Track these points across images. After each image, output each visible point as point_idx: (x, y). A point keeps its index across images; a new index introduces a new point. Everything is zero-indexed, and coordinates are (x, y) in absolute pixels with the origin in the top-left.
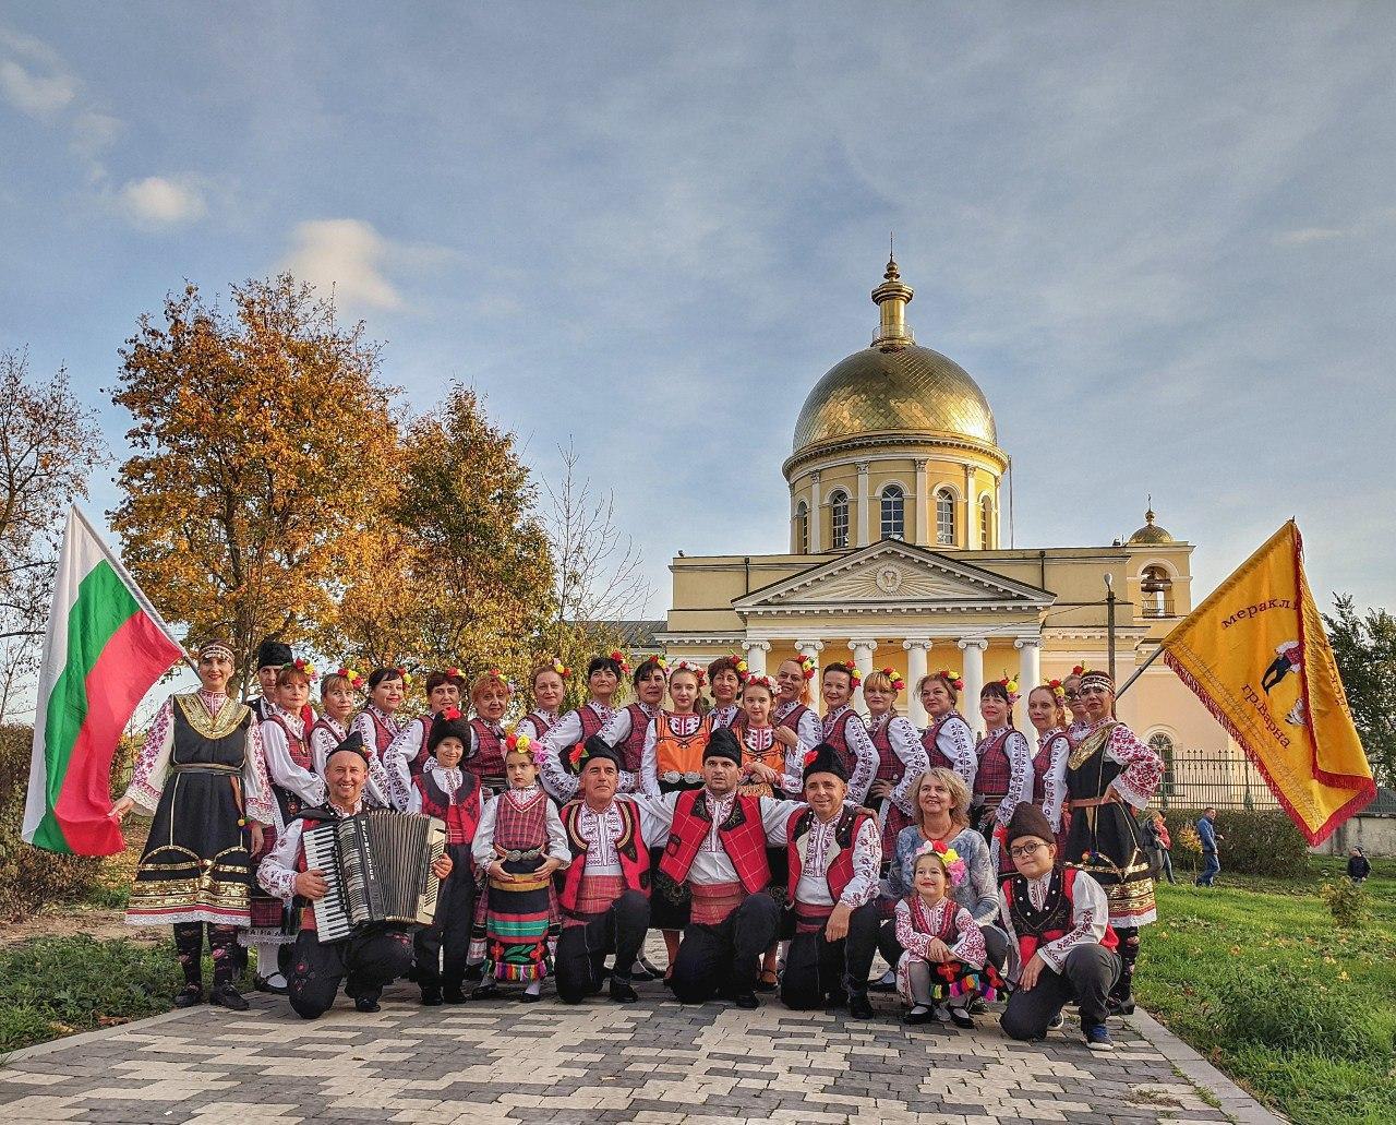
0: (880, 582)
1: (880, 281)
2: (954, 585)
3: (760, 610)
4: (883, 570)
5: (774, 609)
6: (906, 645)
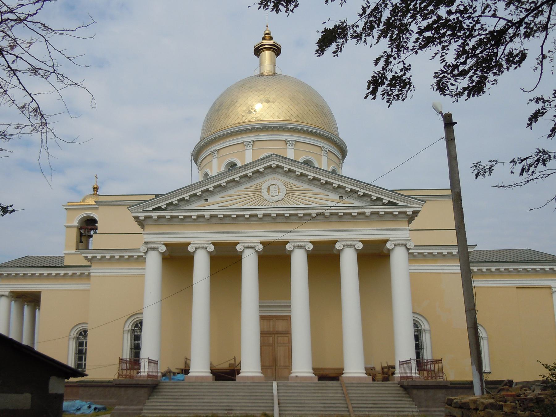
3: (155, 215)
5: (168, 214)
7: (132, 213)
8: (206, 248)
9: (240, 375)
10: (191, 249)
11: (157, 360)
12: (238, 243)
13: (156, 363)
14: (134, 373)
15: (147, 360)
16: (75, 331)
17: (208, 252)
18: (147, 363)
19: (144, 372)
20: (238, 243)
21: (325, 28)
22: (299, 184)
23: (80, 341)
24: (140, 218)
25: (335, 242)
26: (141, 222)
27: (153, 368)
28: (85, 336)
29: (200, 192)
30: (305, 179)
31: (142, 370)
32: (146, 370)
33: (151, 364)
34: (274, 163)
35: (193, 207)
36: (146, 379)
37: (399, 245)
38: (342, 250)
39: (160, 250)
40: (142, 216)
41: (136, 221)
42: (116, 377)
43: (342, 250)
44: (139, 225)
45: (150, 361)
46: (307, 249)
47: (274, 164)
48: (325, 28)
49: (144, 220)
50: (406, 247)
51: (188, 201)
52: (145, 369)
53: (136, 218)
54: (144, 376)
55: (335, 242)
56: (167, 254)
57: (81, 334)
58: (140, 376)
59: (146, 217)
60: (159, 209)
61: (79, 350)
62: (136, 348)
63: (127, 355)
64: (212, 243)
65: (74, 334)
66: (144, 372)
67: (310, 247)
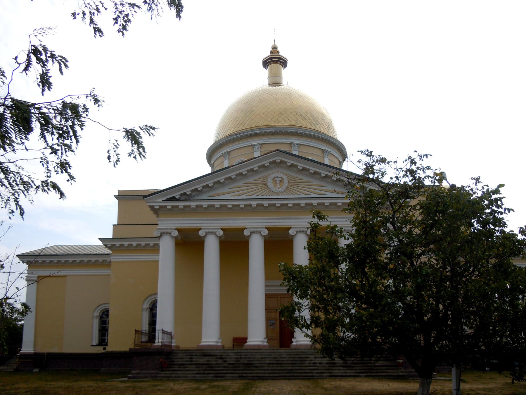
0: (270, 184)
1: (267, 54)
2: (330, 187)
3: (169, 204)
4: (273, 176)
5: (181, 204)
6: (291, 232)
7: (147, 203)
8: (171, 233)
9: (246, 344)
10: (246, 233)
11: (171, 332)
12: (245, 228)
13: (170, 334)
14: (149, 344)
15: (161, 331)
16: (99, 310)
17: (172, 237)
18: (160, 334)
19: (158, 342)
20: (245, 228)
21: (116, 196)
22: (300, 177)
23: (103, 319)
24: (155, 207)
25: (290, 228)
26: (156, 211)
27: (166, 341)
28: (107, 316)
29: (268, 163)
30: (307, 173)
31: (156, 341)
32: (160, 341)
33: (165, 335)
34: (278, 159)
35: (205, 197)
36: (160, 347)
37: (300, 232)
38: (295, 235)
39: (172, 234)
40: (157, 205)
41: (152, 210)
42: (133, 347)
43: (295, 235)
44: (154, 213)
45: (164, 332)
46: (263, 234)
47: (278, 159)
48: (116, 196)
49: (158, 209)
50: (171, 235)
51: (200, 192)
52: (159, 341)
53: (152, 208)
54: (158, 346)
55: (290, 228)
56: (179, 238)
57: (103, 313)
58: (155, 346)
59: (161, 207)
60: (173, 199)
61: (102, 327)
62: (153, 323)
63: (145, 327)
64: (221, 229)
65: (97, 314)
66: (158, 342)
67: (265, 232)
